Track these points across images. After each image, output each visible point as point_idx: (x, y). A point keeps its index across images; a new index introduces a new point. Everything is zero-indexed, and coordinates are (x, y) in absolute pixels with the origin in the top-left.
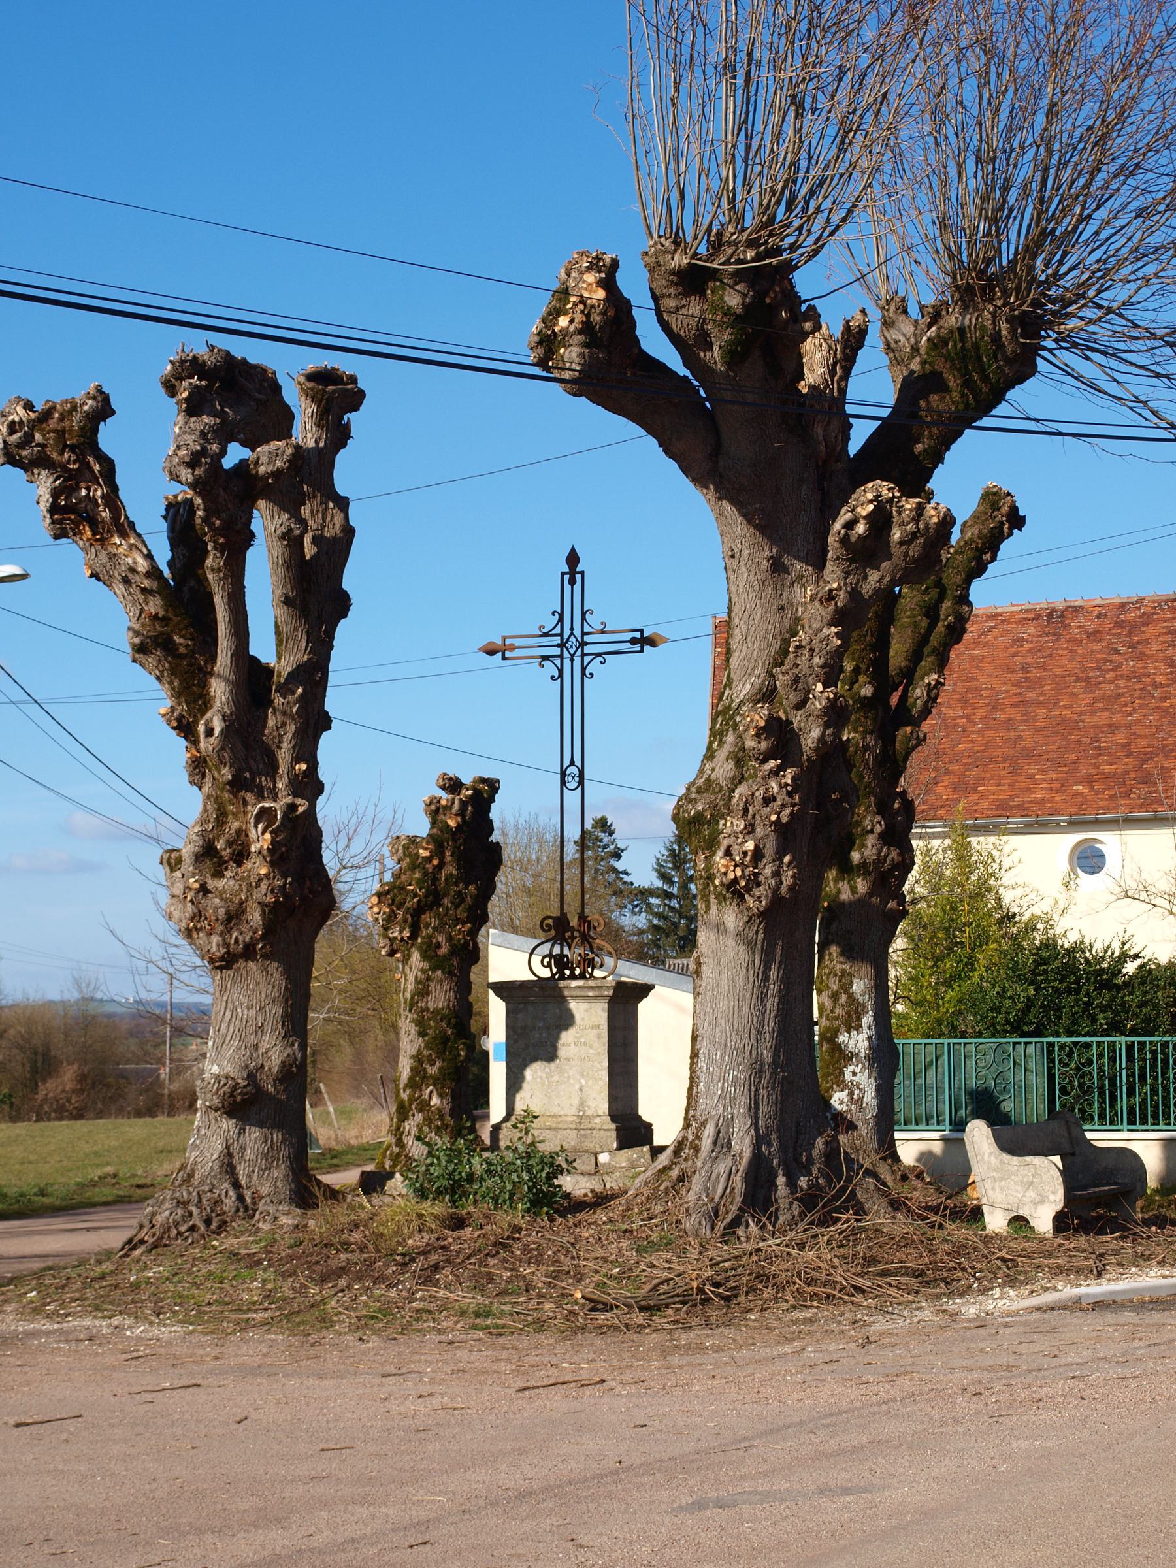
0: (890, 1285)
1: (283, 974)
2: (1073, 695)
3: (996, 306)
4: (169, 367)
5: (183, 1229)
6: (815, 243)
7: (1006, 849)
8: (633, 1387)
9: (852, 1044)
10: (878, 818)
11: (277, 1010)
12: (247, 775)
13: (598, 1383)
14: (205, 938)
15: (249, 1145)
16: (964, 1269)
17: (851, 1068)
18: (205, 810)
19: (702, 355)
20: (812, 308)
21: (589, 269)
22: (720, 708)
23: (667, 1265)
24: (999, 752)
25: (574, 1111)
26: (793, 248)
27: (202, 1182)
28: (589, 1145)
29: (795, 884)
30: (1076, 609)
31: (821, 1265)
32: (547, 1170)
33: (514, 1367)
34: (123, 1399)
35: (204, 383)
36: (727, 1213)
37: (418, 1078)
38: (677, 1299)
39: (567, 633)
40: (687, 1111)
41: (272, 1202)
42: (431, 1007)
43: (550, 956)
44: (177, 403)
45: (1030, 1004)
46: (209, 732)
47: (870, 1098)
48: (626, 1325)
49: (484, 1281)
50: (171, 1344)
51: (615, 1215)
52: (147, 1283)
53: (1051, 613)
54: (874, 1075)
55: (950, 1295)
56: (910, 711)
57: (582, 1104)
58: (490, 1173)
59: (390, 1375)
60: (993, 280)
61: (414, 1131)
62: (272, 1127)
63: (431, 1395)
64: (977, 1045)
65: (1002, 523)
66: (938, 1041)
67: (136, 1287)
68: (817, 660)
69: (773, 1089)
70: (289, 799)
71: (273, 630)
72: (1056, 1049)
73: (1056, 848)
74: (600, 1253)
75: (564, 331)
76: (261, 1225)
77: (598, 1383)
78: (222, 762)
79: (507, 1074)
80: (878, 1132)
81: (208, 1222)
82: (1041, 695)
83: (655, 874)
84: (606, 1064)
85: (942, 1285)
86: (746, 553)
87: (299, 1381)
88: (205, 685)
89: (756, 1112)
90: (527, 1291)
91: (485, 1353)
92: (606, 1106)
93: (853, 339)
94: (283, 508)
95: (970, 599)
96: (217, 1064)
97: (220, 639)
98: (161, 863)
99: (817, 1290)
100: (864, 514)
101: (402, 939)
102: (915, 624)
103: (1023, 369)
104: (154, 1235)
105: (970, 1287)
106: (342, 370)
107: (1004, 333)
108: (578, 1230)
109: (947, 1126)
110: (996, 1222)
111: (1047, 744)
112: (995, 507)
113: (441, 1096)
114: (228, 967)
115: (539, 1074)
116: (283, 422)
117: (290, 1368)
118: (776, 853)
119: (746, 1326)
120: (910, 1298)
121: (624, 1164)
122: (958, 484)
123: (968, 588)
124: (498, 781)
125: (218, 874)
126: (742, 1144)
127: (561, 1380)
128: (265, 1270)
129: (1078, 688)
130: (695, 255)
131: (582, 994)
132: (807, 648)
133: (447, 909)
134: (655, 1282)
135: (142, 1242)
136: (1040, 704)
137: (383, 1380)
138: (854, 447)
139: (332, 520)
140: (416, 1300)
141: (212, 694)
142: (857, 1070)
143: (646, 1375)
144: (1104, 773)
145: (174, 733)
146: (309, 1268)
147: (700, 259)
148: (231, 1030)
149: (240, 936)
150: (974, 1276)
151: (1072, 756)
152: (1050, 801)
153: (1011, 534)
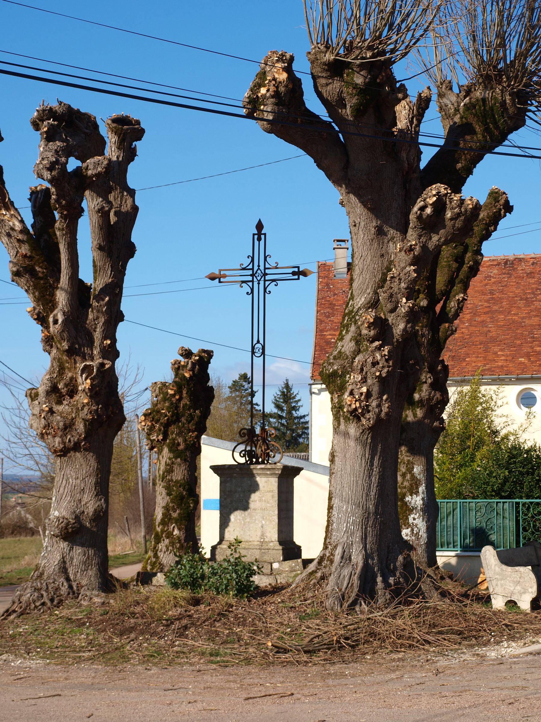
0: (445, 639)
1: (96, 460)
2: (519, 308)
3: (503, 86)
4: (36, 114)
5: (38, 604)
6: (406, 49)
7: (501, 395)
8: (311, 698)
9: (413, 501)
10: (429, 375)
11: (92, 481)
12: (77, 346)
13: (290, 695)
14: (52, 439)
15: (76, 557)
16: (485, 630)
17: (412, 516)
18: (52, 366)
19: (340, 111)
20: (403, 86)
21: (278, 61)
22: (346, 311)
23: (317, 627)
24: (477, 339)
25: (258, 539)
26: (393, 51)
27: (49, 578)
28: (267, 558)
29: (389, 411)
30: (520, 260)
31: (406, 628)
32: (247, 572)
33: (239, 686)
34: (18, 703)
35: (56, 123)
36: (349, 597)
37: (166, 519)
38: (325, 647)
39: (256, 268)
40: (325, 539)
41: (88, 589)
42: (174, 479)
43: (245, 450)
44: (41, 134)
45: (506, 480)
46: (56, 322)
47: (423, 534)
48: (297, 661)
49: (214, 636)
50: (38, 670)
51: (286, 598)
52: (20, 635)
53: (506, 262)
54: (425, 519)
55: (479, 645)
56: (447, 314)
57: (263, 535)
58: (214, 574)
59: (169, 690)
60: (502, 71)
61: (164, 549)
62: (89, 546)
63: (195, 701)
64: (476, 503)
65: (500, 210)
66: (454, 501)
67: (13, 637)
68: (403, 285)
69: (375, 527)
70: (100, 360)
71: (92, 264)
72: (521, 505)
73: (511, 392)
74: (279, 620)
75: (264, 96)
76: (82, 602)
77: (290, 695)
78: (63, 339)
79: (220, 518)
80: (427, 552)
81: (52, 600)
82: (501, 307)
83: (273, 405)
84: (276, 512)
85: (473, 639)
86: (362, 224)
87: (117, 693)
88: (53, 295)
89: (366, 541)
90: (239, 641)
91: (220, 677)
92: (276, 536)
93: (423, 104)
94: (99, 195)
95: (482, 252)
96: (59, 511)
97: (62, 269)
98: (26, 396)
99: (405, 642)
100: (431, 202)
101: (158, 440)
102: (449, 266)
103: (518, 122)
104: (21, 607)
105: (489, 641)
106: (131, 117)
107: (508, 101)
108: (265, 606)
109: (459, 548)
110: (498, 603)
111: (504, 335)
112: (497, 200)
113: (179, 529)
114: (64, 455)
115: (239, 517)
116: (99, 145)
117: (110, 685)
118: (379, 394)
119: (366, 662)
120: (456, 647)
121: (287, 569)
122: (476, 189)
123: (481, 246)
124: (212, 352)
125: (59, 403)
126: (358, 558)
127: (268, 694)
128: (87, 628)
129: (521, 304)
130: (338, 54)
131: (264, 472)
132: (398, 278)
133: (184, 424)
134: (313, 636)
135: (14, 611)
136: (500, 312)
137: (165, 692)
138: (423, 164)
139: (125, 202)
140: (176, 646)
141: (57, 300)
142: (416, 517)
143: (316, 691)
144: (536, 352)
145: (35, 322)
146: (113, 627)
147: (340, 57)
149: (72, 438)
150: (491, 634)
151: (518, 342)
152: (507, 367)
153: (505, 216)
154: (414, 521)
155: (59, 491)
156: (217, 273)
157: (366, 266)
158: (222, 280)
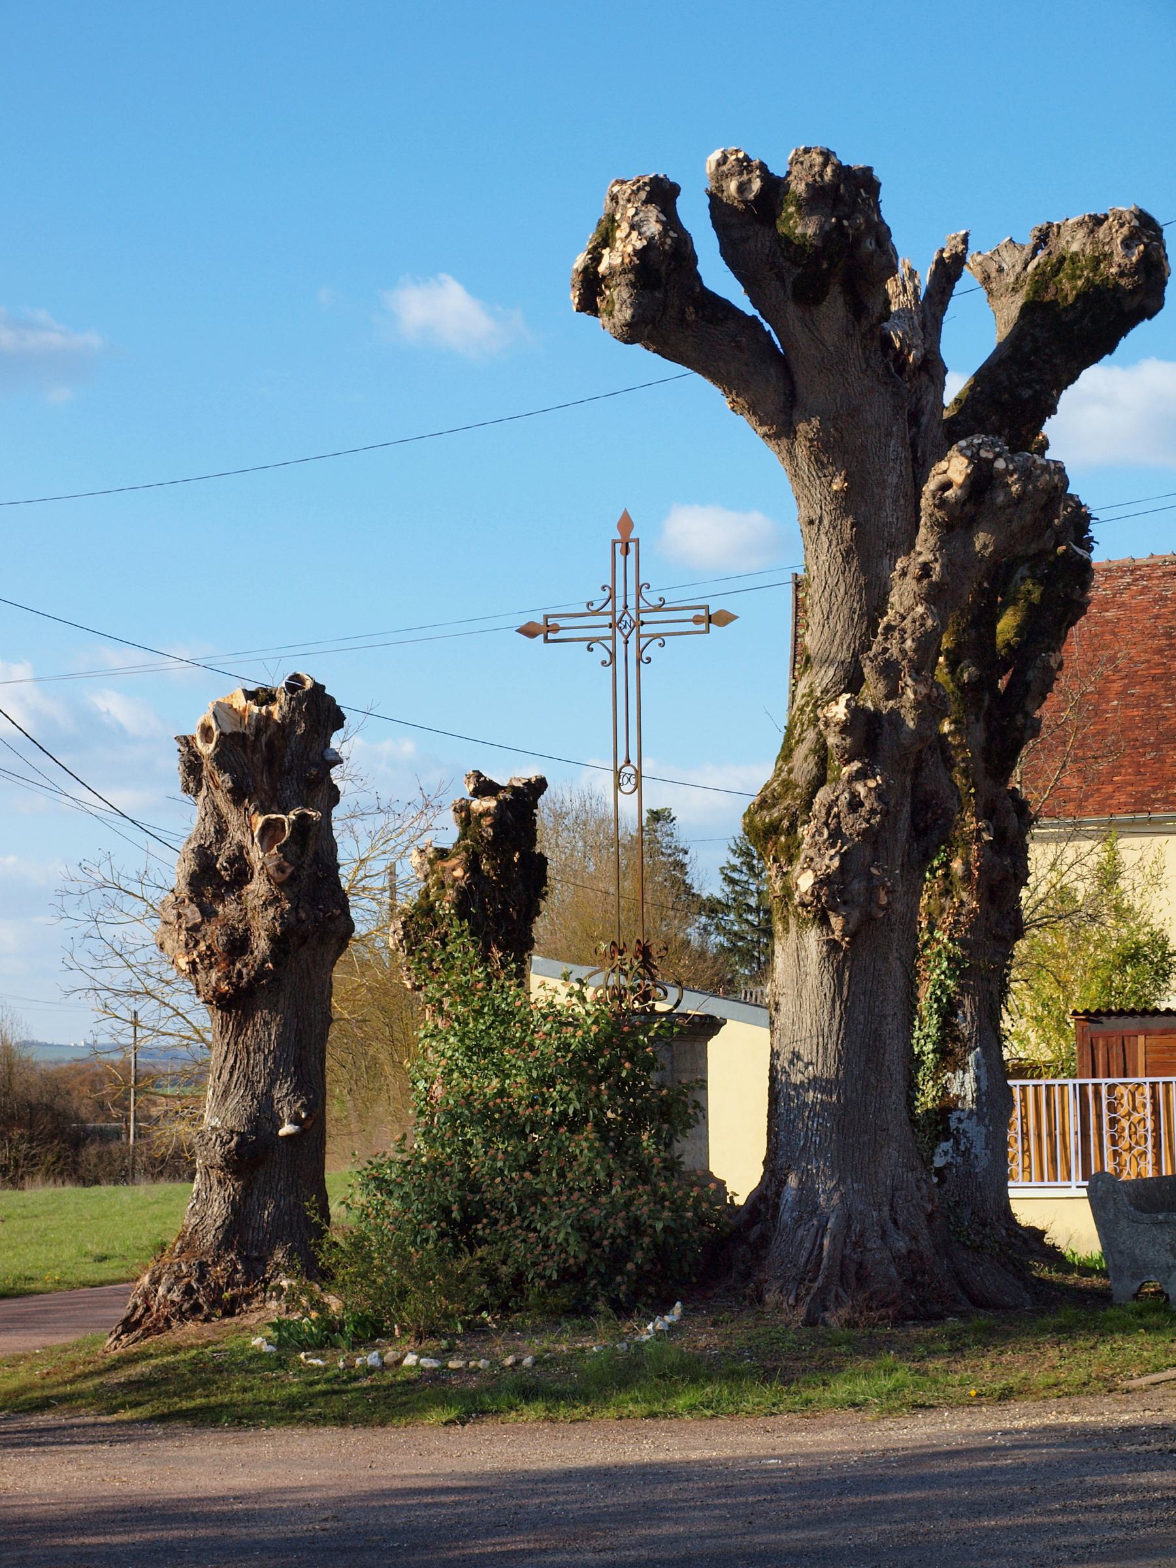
39: (632, 639)
68: (909, 643)
148: (235, 1077)
155: (219, 1078)
156: (540, 620)
157: (835, 608)
158: (551, 636)
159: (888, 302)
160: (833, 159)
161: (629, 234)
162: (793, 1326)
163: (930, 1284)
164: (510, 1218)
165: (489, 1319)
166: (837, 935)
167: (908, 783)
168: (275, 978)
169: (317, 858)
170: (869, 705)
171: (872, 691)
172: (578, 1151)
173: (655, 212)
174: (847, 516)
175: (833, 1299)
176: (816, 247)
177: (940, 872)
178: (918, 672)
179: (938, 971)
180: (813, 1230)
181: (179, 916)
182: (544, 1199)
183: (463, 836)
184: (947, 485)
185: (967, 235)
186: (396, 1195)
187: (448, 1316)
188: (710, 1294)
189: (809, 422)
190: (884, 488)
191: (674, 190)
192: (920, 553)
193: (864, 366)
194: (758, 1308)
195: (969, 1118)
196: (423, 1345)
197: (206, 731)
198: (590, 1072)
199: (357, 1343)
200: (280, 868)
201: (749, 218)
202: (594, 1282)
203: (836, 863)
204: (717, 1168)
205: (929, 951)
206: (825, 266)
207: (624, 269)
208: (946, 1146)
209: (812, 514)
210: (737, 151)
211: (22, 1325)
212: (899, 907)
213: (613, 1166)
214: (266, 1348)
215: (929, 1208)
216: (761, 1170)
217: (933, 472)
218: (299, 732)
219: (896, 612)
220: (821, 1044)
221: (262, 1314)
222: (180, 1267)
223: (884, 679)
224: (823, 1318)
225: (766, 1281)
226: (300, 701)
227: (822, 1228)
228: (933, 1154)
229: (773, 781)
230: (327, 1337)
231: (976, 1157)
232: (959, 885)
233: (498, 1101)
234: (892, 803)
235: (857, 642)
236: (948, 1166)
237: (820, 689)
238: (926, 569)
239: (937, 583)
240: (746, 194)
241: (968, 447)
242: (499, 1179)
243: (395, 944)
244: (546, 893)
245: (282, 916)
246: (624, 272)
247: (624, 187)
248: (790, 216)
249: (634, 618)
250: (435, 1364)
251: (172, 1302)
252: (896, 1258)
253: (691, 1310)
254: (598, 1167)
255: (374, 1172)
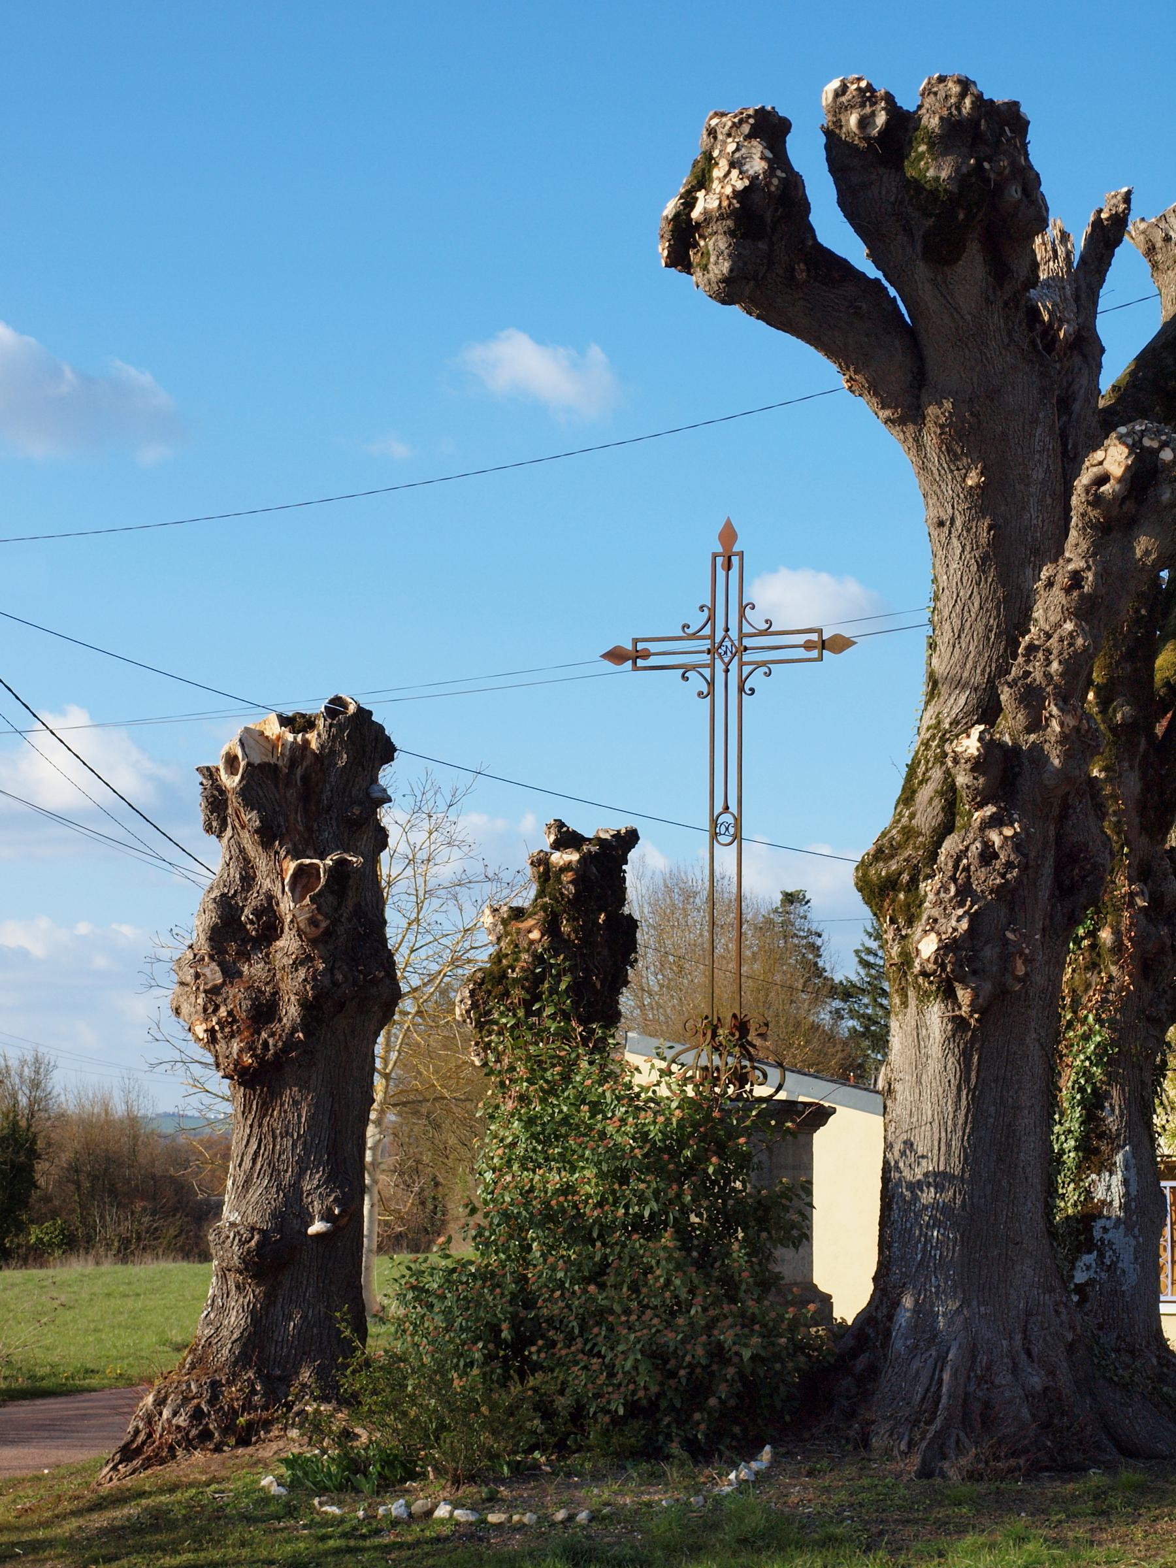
39: (734, 667)
68: (1055, 665)
154: (1105, 1236)
155: (240, 1166)
157: (968, 624)
158: (640, 663)
159: (1035, 266)
160: (973, 89)
161: (729, 172)
162: (905, 1478)
163: (1068, 1428)
164: (570, 1339)
165: (543, 1459)
166: (965, 1011)
167: (1052, 832)
168: (307, 1049)
169: (358, 912)
170: (1007, 738)
171: (1011, 723)
172: (653, 1262)
173: (760, 148)
174: (984, 517)
175: (953, 1446)
176: (951, 192)
177: (1086, 943)
178: (1065, 700)
179: (1082, 1057)
180: (931, 1361)
181: (197, 976)
182: (611, 1319)
183: (541, 894)
184: (1104, 479)
185: (1129, 193)
186: (436, 1309)
187: (493, 1456)
188: (807, 1435)
189: (940, 405)
190: (1028, 485)
191: (784, 126)
192: (1069, 560)
193: (1006, 340)
194: (864, 1454)
195: (1116, 1227)
196: (460, 1493)
197: (231, 761)
198: (671, 1167)
199: (386, 1486)
200: (312, 922)
201: (872, 157)
202: (667, 1419)
203: (964, 925)
204: (822, 1279)
205: (1071, 1033)
206: (961, 216)
207: (721, 215)
208: (1089, 1258)
209: (942, 514)
210: (859, 80)
211: (46, 1434)
212: (1039, 980)
213: (696, 1282)
214: (275, 1490)
215: (1070, 1337)
216: (870, 1287)
217: (1087, 463)
218: (340, 764)
219: (1040, 630)
220: (943, 1140)
221: (281, 1444)
222: (189, 1386)
223: (1025, 707)
224: (941, 1468)
225: (873, 1422)
226: (341, 728)
227: (942, 1360)
228: (1073, 1268)
229: (892, 828)
230: (348, 1480)
231: (1124, 1272)
232: (1107, 958)
233: (561, 1199)
234: (1033, 855)
235: (994, 665)
236: (1091, 1282)
237: (948, 720)
238: (1076, 579)
239: (1090, 595)
240: (869, 130)
241: (1128, 434)
242: (558, 1293)
243: (462, 1015)
244: (636, 960)
245: (314, 978)
246: (722, 217)
247: (724, 119)
248: (921, 156)
249: (736, 643)
250: (472, 1518)
251: (178, 1427)
252: (1029, 1396)
253: (783, 1456)
254: (678, 1282)
255: (413, 1280)
